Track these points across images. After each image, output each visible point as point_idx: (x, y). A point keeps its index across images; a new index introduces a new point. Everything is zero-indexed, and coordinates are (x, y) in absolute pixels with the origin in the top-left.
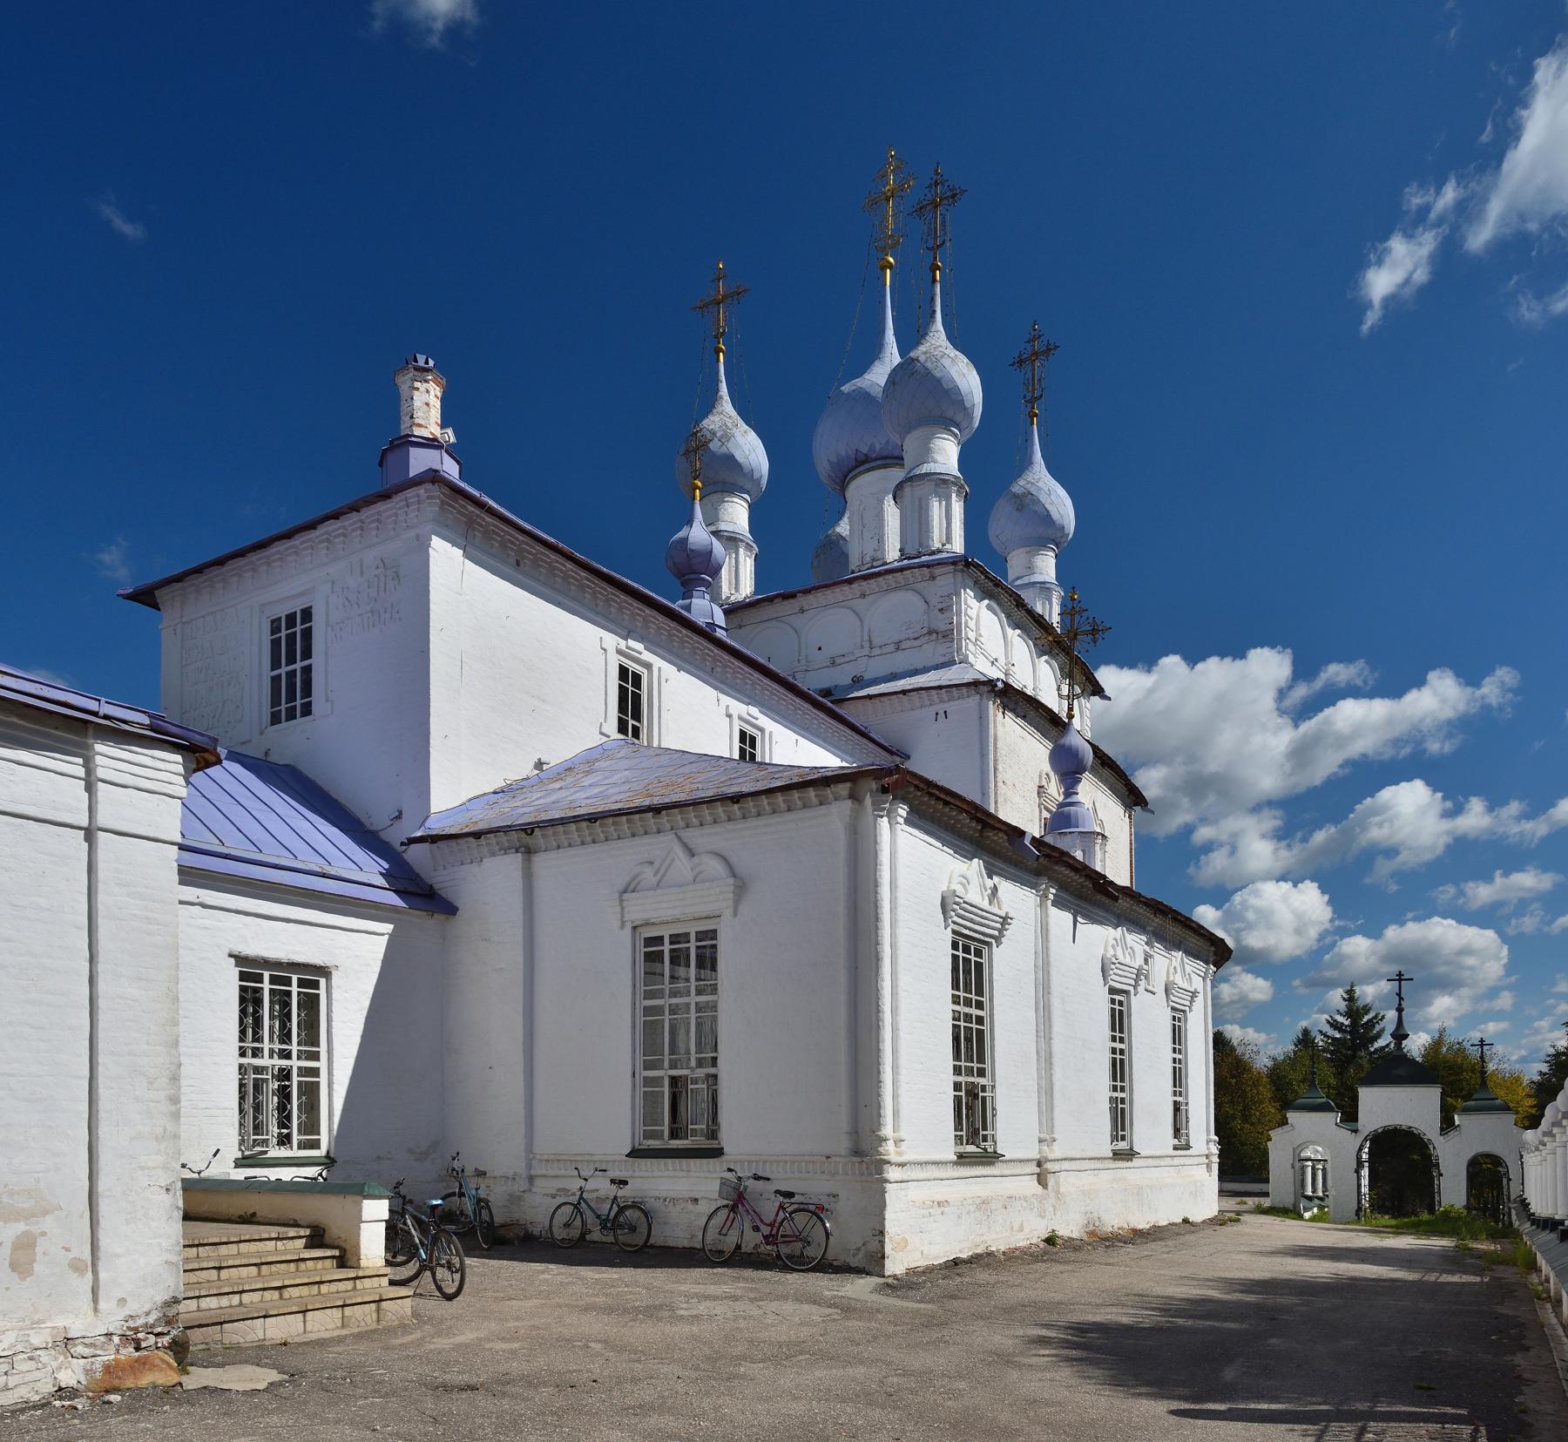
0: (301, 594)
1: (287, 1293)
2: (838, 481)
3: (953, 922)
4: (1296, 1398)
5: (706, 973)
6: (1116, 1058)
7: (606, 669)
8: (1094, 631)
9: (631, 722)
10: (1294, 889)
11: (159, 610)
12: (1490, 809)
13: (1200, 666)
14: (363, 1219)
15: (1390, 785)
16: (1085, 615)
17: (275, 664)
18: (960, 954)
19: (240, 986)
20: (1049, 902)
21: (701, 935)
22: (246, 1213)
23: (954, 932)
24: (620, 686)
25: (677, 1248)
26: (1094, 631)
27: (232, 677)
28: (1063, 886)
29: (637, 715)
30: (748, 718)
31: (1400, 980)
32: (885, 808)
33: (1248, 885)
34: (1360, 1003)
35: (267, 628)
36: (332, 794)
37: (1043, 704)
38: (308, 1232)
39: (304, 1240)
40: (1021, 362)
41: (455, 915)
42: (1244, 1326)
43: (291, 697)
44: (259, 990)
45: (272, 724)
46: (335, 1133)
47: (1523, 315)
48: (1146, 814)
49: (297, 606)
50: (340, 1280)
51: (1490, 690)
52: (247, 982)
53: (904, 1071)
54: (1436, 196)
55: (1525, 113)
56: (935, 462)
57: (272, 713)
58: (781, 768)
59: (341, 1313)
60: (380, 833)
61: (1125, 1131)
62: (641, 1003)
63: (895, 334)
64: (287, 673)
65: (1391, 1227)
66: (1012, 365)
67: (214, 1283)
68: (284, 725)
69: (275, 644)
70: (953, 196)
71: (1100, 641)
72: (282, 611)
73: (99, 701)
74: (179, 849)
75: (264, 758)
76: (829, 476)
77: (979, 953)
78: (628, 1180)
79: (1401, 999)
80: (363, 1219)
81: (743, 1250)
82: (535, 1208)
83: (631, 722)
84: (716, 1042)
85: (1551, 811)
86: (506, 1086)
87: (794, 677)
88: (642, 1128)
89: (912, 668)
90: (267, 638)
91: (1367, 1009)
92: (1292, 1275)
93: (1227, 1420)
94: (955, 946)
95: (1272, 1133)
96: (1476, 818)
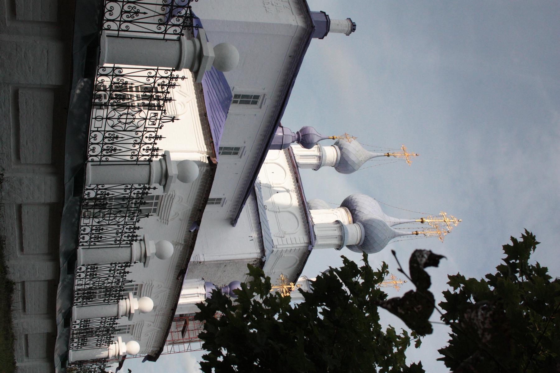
0: (223, 204)
1: (411, 233)
2: (345, 204)
3: (166, 195)
6: (126, 330)
7: (145, 245)
9: (239, 100)
10: (442, 291)
12: (456, 293)
13: (546, 267)
18: (127, 327)
20: (499, 272)
22: (513, 239)
23: (163, 196)
24: (251, 104)
25: (71, 89)
29: (242, 102)
30: (265, 99)
33: (43, 280)
39: (168, 14)
41: (214, 49)
42: (75, 99)
47: (126, 341)
50: (215, 81)
51: (524, 316)
52: (149, 209)
54: (449, 334)
56: (415, 341)
67: (89, 208)
76: (523, 235)
77: (128, 332)
83: (239, 100)
85: (55, 202)
92: (348, 212)
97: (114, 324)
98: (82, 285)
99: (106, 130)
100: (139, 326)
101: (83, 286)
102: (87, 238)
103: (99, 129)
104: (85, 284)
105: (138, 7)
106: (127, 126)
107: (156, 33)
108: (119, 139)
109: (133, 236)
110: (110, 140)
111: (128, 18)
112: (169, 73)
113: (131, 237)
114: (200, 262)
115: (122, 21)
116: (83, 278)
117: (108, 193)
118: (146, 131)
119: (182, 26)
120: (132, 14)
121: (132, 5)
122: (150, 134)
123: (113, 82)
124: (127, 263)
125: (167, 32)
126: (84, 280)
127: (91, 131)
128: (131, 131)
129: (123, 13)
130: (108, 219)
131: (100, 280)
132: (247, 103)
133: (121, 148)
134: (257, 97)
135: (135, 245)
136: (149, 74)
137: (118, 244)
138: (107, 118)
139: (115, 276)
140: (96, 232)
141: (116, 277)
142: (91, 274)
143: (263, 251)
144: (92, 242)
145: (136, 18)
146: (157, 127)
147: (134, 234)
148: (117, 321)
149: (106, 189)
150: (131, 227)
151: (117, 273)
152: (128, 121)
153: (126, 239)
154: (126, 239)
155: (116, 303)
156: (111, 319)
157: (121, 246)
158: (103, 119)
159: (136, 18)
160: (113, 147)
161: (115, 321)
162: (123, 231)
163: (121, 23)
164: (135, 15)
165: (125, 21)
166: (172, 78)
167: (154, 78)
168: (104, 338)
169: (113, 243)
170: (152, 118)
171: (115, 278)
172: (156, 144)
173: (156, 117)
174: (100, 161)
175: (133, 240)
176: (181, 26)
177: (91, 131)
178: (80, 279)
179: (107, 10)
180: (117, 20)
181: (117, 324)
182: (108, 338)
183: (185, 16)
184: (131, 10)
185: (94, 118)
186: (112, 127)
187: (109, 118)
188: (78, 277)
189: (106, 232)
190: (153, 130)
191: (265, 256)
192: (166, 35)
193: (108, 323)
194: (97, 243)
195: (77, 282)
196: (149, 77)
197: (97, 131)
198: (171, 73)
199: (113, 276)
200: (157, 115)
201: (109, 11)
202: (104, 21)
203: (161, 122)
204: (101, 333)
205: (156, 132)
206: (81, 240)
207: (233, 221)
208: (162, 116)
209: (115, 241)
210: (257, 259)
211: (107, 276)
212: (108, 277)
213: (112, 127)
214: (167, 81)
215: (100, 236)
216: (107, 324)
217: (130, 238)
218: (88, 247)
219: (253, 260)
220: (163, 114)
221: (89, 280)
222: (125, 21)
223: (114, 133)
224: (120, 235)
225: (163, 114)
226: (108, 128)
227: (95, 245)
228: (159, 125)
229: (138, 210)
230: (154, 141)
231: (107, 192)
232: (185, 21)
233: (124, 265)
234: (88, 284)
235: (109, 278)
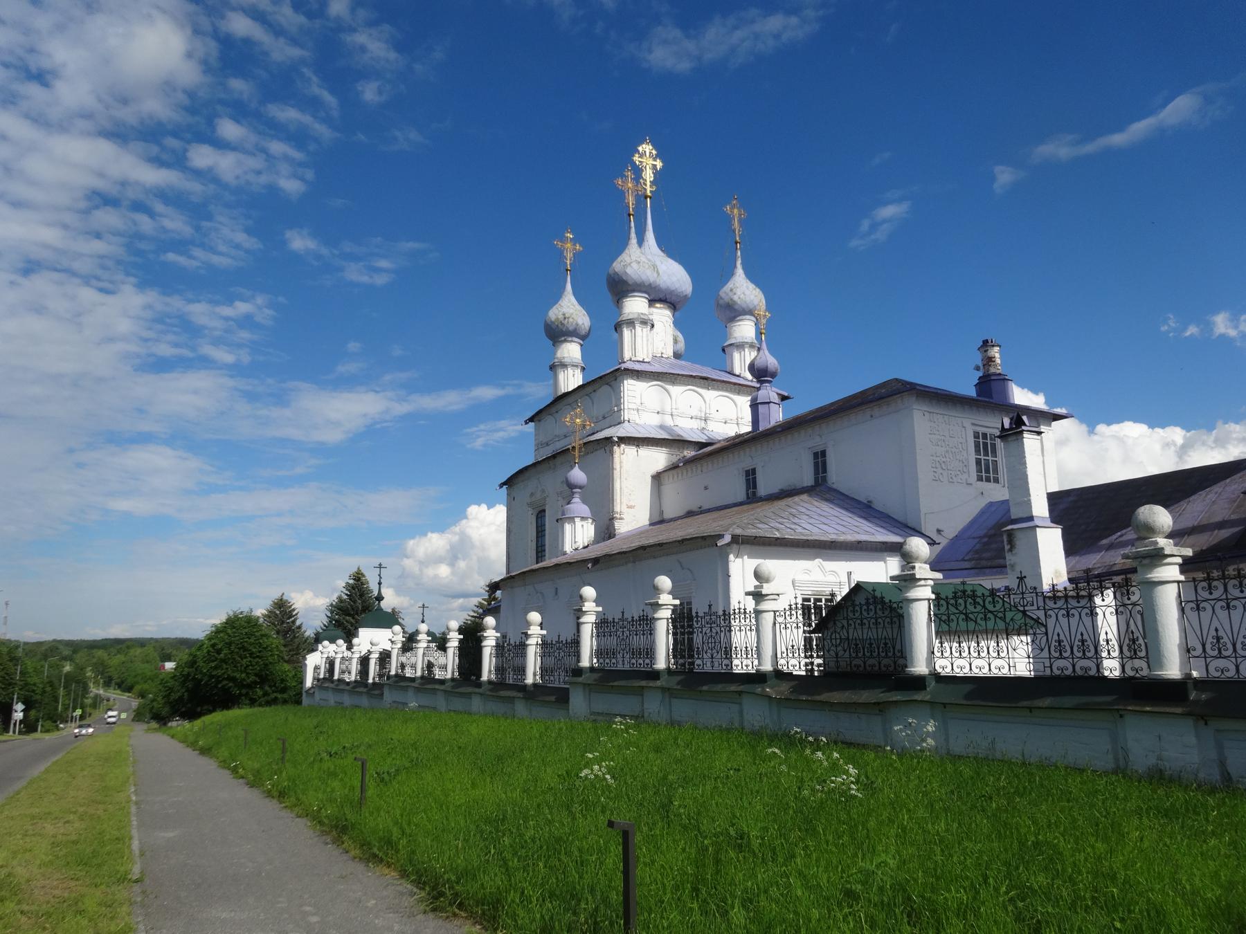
4: (1015, 440)
5: (514, 638)
6: (984, 455)
11: (501, 485)
15: (1135, 421)
19: (976, 458)
28: (644, 286)
31: (380, 568)
35: (811, 457)
36: (731, 594)
37: (653, 438)
38: (672, 607)
44: (983, 439)
53: (1148, 508)
55: (914, 398)
58: (883, 519)
60: (741, 559)
62: (11, 736)
75: (1129, 576)
79: (381, 578)
82: (68, 835)
84: (1042, 725)
88: (999, 476)
93: (918, 492)
95: (307, 656)
99: (1048, 657)
103: (849, 663)
105: (1077, 643)
106: (829, 641)
108: (727, 646)
115: (1235, 655)
118: (1044, 607)
127: (1208, 677)
128: (848, 633)
130: (710, 641)
131: (717, 644)
133: (1213, 628)
138: (712, 658)
160: (1078, 645)
177: (1208, 677)
180: (1096, 662)
186: (845, 651)
187: (712, 656)
195: (620, 667)
197: (1051, 667)
201: (1222, 672)
202: (1126, 675)
203: (1027, 592)
206: (861, 669)
211: (700, 635)
213: (845, 651)
226: (719, 656)
228: (1032, 593)
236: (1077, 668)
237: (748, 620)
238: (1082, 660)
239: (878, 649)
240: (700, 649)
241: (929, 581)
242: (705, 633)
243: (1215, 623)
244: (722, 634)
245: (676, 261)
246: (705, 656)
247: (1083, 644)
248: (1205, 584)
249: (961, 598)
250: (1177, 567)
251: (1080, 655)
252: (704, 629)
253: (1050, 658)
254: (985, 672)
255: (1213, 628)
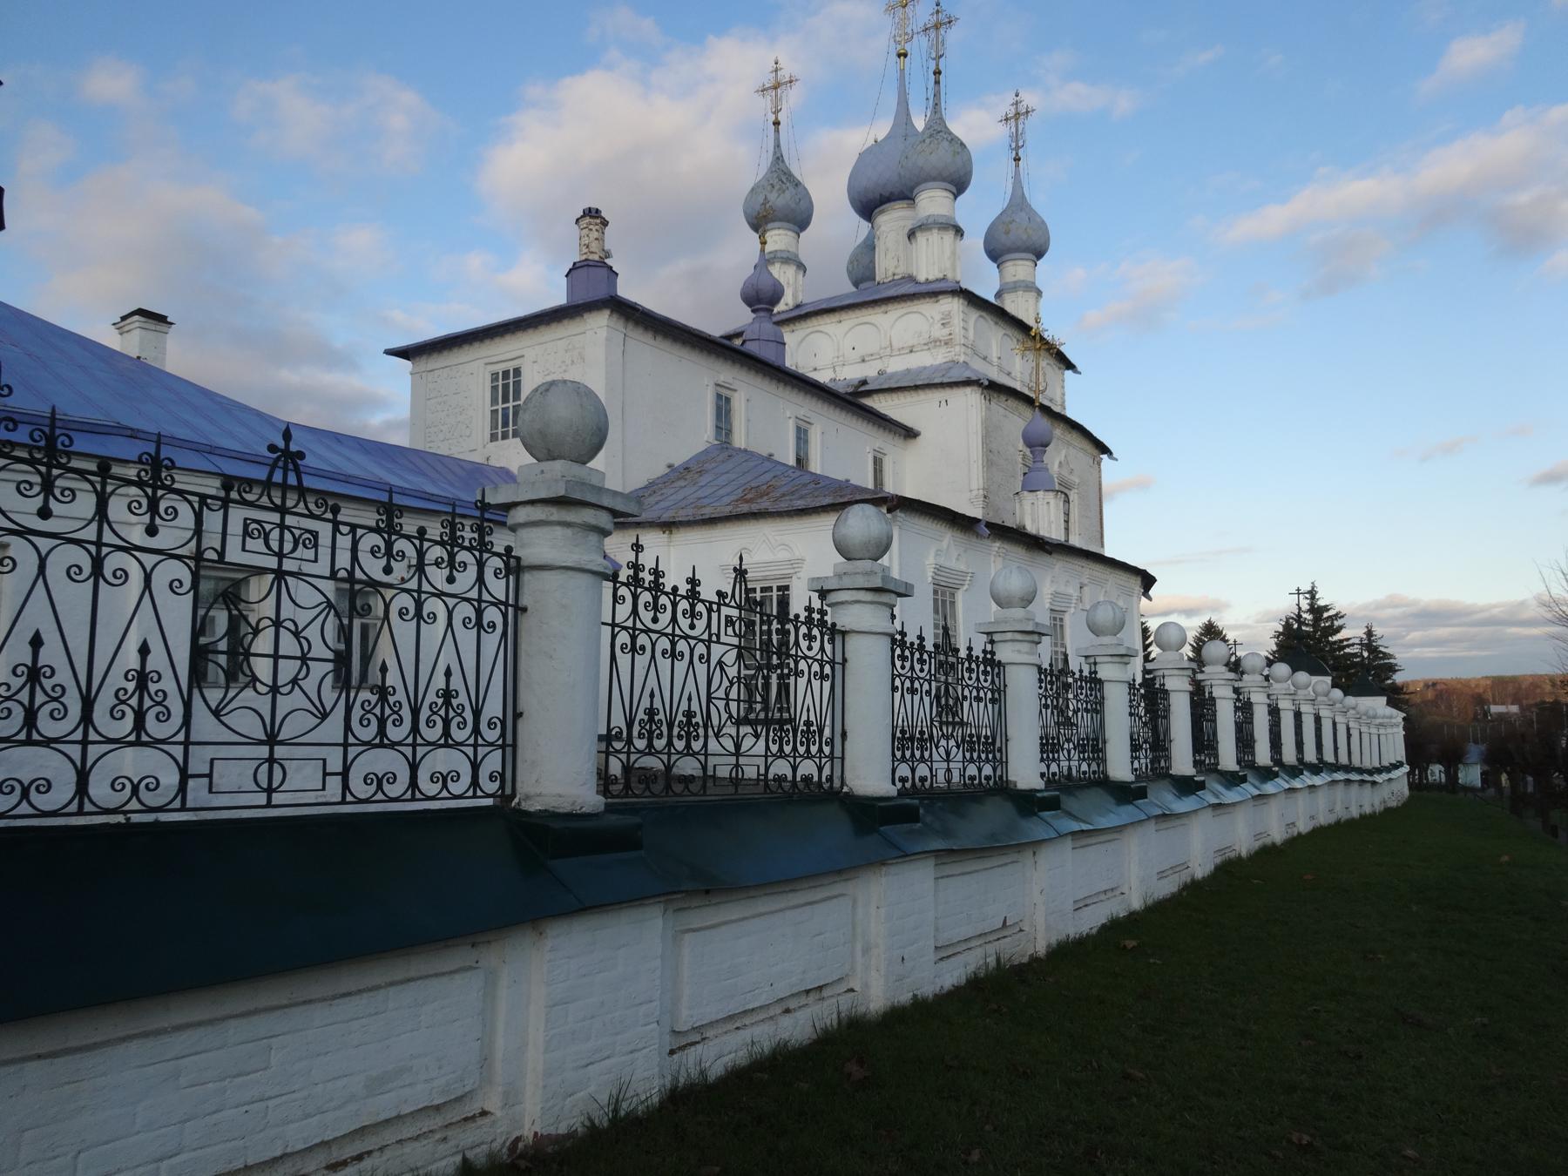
8: (1027, 112)
14: (340, 777)
16: (945, 13)
17: (494, 401)
19: (509, 370)
21: (779, 588)
26: (1006, 120)
27: (36, 642)
32: (1152, 642)
34: (1321, 603)
35: (488, 378)
40: (1006, 120)
43: (506, 387)
45: (491, 441)
46: (78, 477)
48: (1111, 461)
49: (510, 366)
57: (492, 387)
59: (1307, 715)
61: (771, 587)
63: (1230, 871)
64: (508, 402)
65: (1348, 646)
66: (1001, 121)
68: (500, 442)
69: (494, 388)
70: (950, 22)
71: (1001, 124)
72: (500, 368)
73: (715, 766)
74: (506, 523)
75: (486, 463)
78: (307, 453)
80: (340, 777)
81: (879, 140)
86: (452, 1159)
87: (615, 556)
89: (923, 365)
90: (488, 385)
91: (1326, 608)
94: (935, 592)
96: (236, 489)
97: (921, 648)
98: (949, 770)
100: (939, 575)
101: (952, 765)
102: (807, 768)
104: (948, 760)
107: (504, 634)
109: (809, 621)
110: (658, 731)
111: (465, 722)
112: (623, 591)
113: (810, 630)
114: (985, 497)
116: (931, 770)
117: (804, 725)
119: (49, 466)
120: (388, 711)
121: (424, 714)
122: (646, 607)
123: (377, 741)
124: (894, 641)
125: (504, 600)
126: (935, 765)
129: (450, 742)
131: (721, 693)
132: (728, 412)
133: (441, 669)
134: (719, 396)
135: (843, 618)
136: (469, 626)
137: (833, 669)
139: (928, 677)
140: (926, 750)
141: (714, 630)
142: (1052, 752)
143: (967, 383)
144: (820, 750)
145: (400, 695)
146: (330, 526)
147: (802, 619)
148: (911, 638)
149: (630, 725)
150: (804, 636)
151: (810, 648)
152: (288, 645)
153: (816, 645)
154: (816, 645)
155: (1002, 668)
156: (903, 658)
157: (839, 659)
158: (271, 760)
159: (400, 695)
161: (977, 657)
162: (989, 689)
163: (480, 741)
164: (656, 718)
165: (476, 731)
166: (636, 581)
167: (484, 605)
168: (1082, 694)
169: (827, 685)
170: (737, 632)
171: (718, 636)
172: (675, 589)
173: (734, 619)
174: (503, 747)
175: (822, 623)
176: (636, 590)
178: (932, 776)
179: (24, 803)
180: (77, 757)
181: (921, 638)
182: (907, 653)
183: (477, 554)
184: (374, 714)
185: (269, 799)
188: (927, 784)
189: (910, 723)
190: (344, 542)
191: (980, 380)
192: (836, 661)
193: (982, 678)
194: (827, 732)
196: (479, 624)
197: (345, 774)
198: (623, 584)
199: (708, 644)
200: (731, 617)
204: (1070, 703)
205: (360, 532)
207: (909, 434)
208: (733, 604)
209: (823, 677)
210: (982, 394)
211: (701, 669)
212: (930, 695)
214: (646, 597)
215: (900, 736)
216: (986, 681)
217: (815, 632)
218: (837, 763)
219: (983, 401)
220: (727, 601)
221: (937, 748)
222: (476, 731)
223: (637, 723)
224: (917, 685)
225: (727, 601)
227: (832, 740)
229: (719, 605)
230: (667, 594)
231: (641, 715)
232: (467, 544)
233: (898, 651)
234: (948, 753)
235: (713, 662)
236: (99, 790)
237: (665, 618)
238: (129, 750)
239: (415, 712)
240: (698, 719)
241: (1008, 634)
242: (720, 663)
243: (38, 617)
244: (966, 705)
245: (891, 129)
246: (713, 745)
247: (447, 703)
248: (375, 539)
249: (470, 549)
250: (1188, 693)
251: (368, 733)
252: (717, 650)
253: (346, 745)
254: (396, 799)
255: (441, 669)
